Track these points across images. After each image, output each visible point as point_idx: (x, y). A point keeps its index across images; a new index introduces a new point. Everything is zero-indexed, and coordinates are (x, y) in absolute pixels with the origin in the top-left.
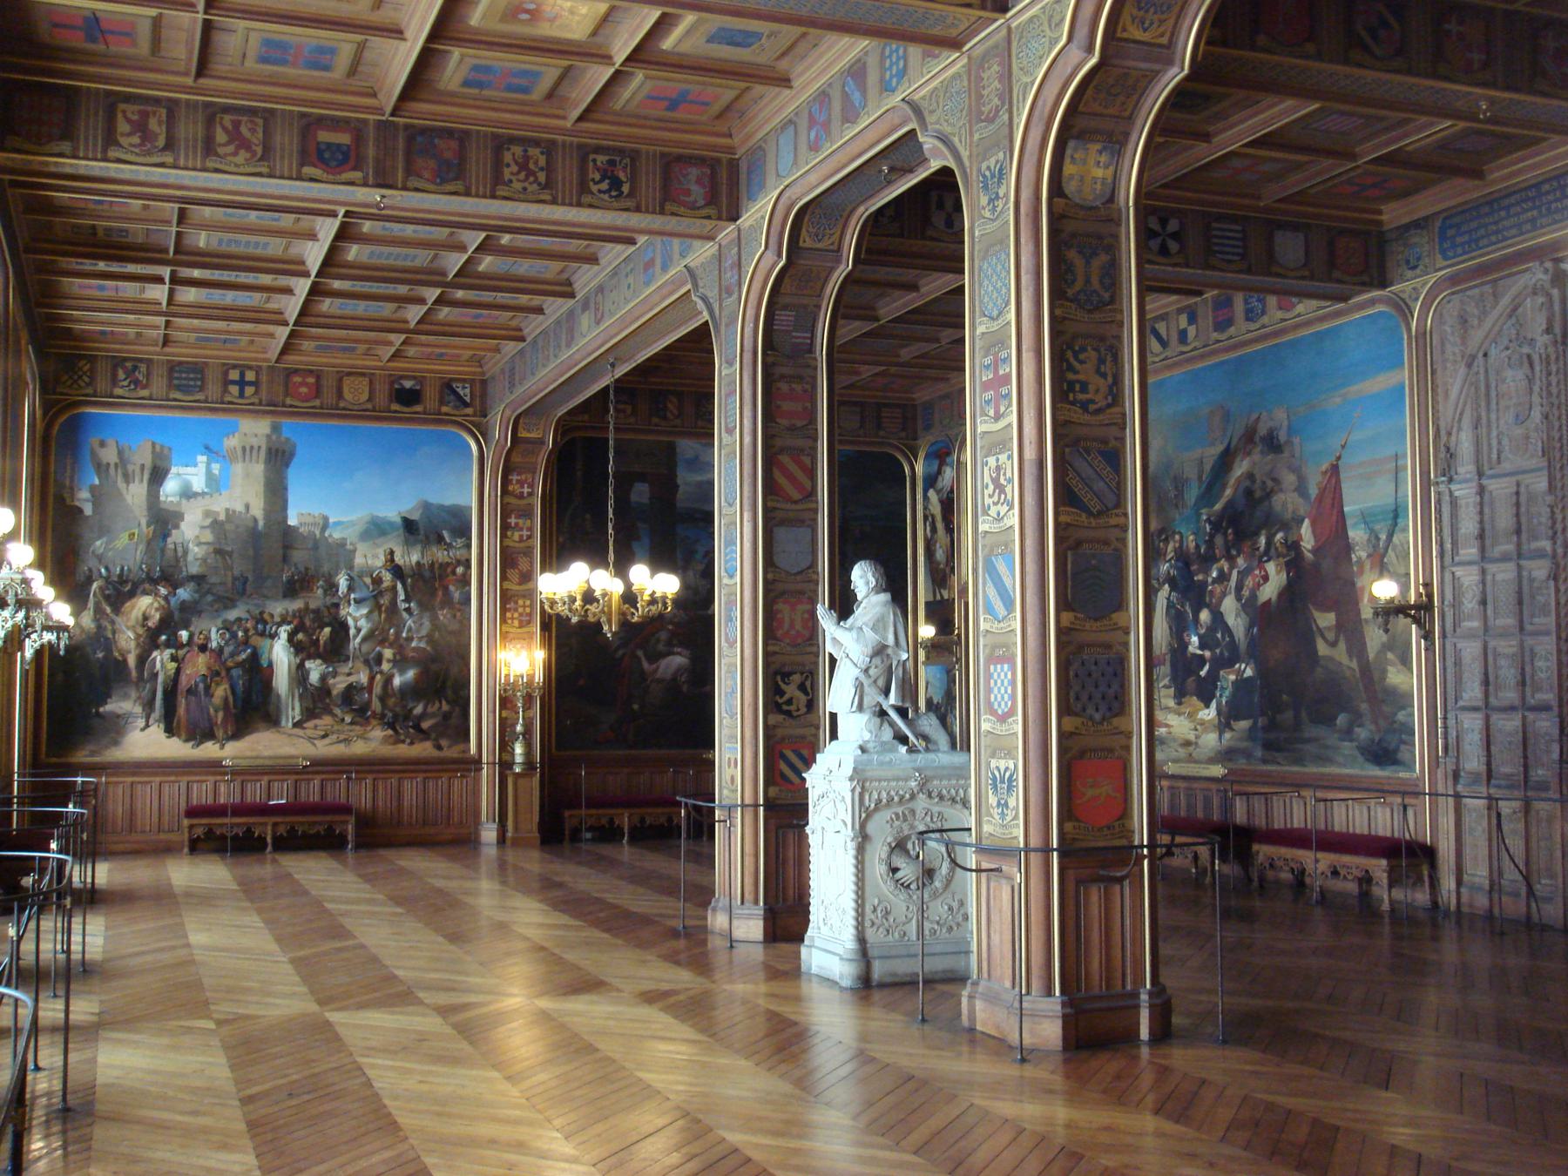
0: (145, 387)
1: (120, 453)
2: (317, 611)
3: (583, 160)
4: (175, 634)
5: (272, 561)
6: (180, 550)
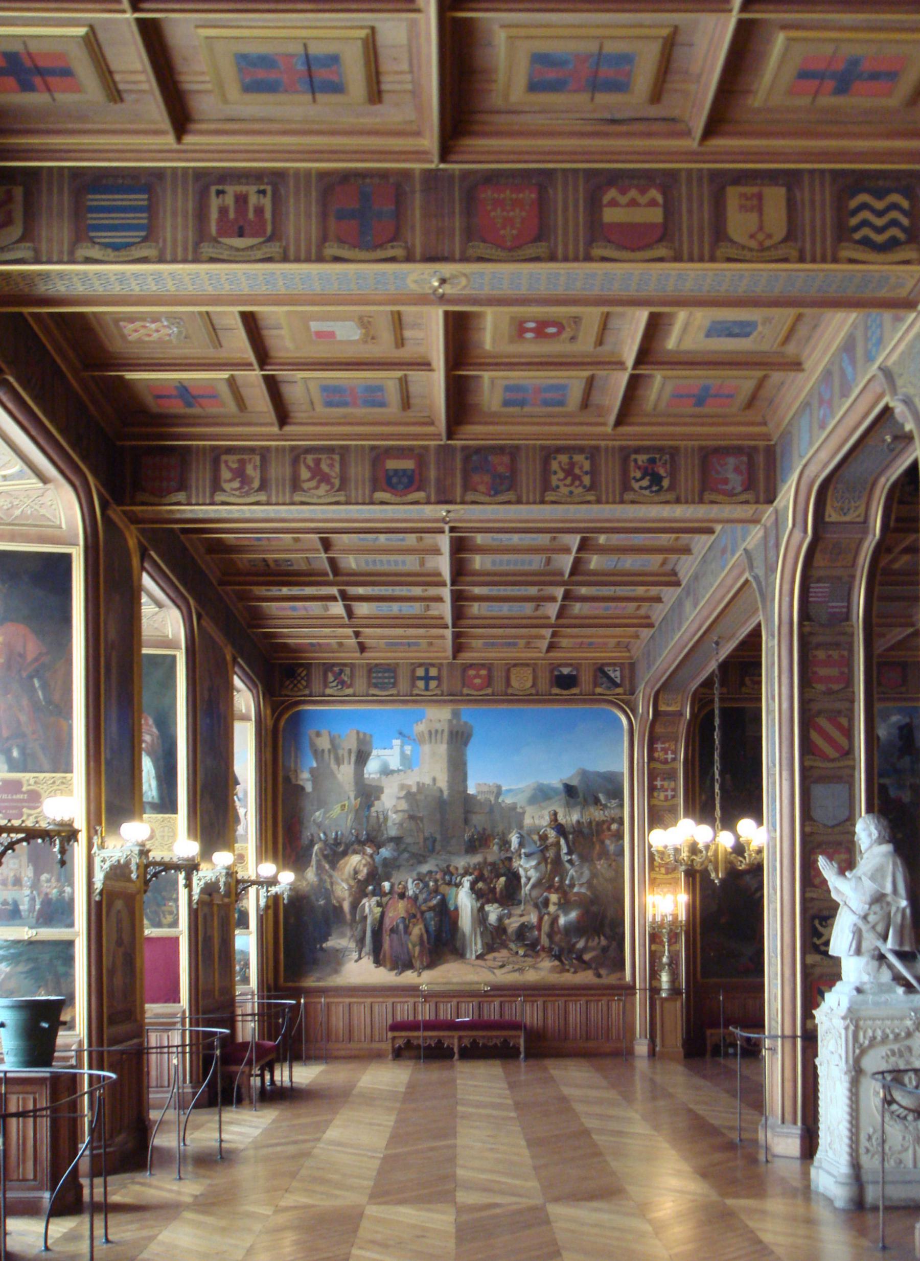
0: (348, 687)
1: (332, 741)
2: (493, 864)
3: (625, 460)
4: (379, 885)
5: (457, 824)
6: (381, 817)
